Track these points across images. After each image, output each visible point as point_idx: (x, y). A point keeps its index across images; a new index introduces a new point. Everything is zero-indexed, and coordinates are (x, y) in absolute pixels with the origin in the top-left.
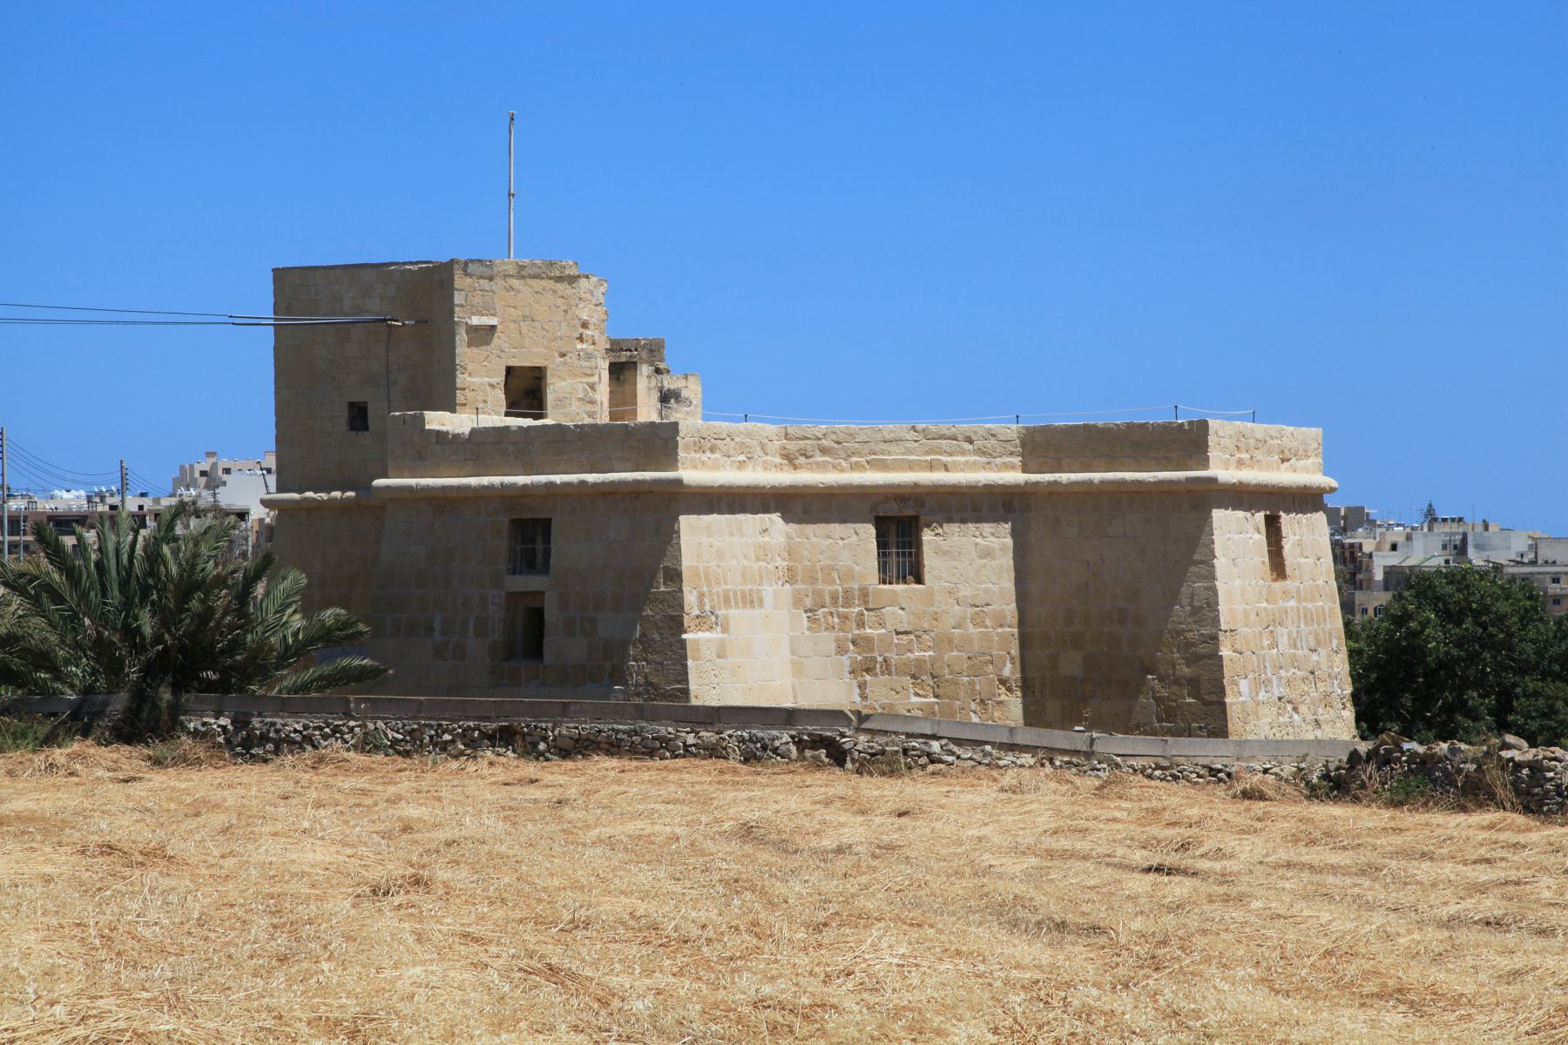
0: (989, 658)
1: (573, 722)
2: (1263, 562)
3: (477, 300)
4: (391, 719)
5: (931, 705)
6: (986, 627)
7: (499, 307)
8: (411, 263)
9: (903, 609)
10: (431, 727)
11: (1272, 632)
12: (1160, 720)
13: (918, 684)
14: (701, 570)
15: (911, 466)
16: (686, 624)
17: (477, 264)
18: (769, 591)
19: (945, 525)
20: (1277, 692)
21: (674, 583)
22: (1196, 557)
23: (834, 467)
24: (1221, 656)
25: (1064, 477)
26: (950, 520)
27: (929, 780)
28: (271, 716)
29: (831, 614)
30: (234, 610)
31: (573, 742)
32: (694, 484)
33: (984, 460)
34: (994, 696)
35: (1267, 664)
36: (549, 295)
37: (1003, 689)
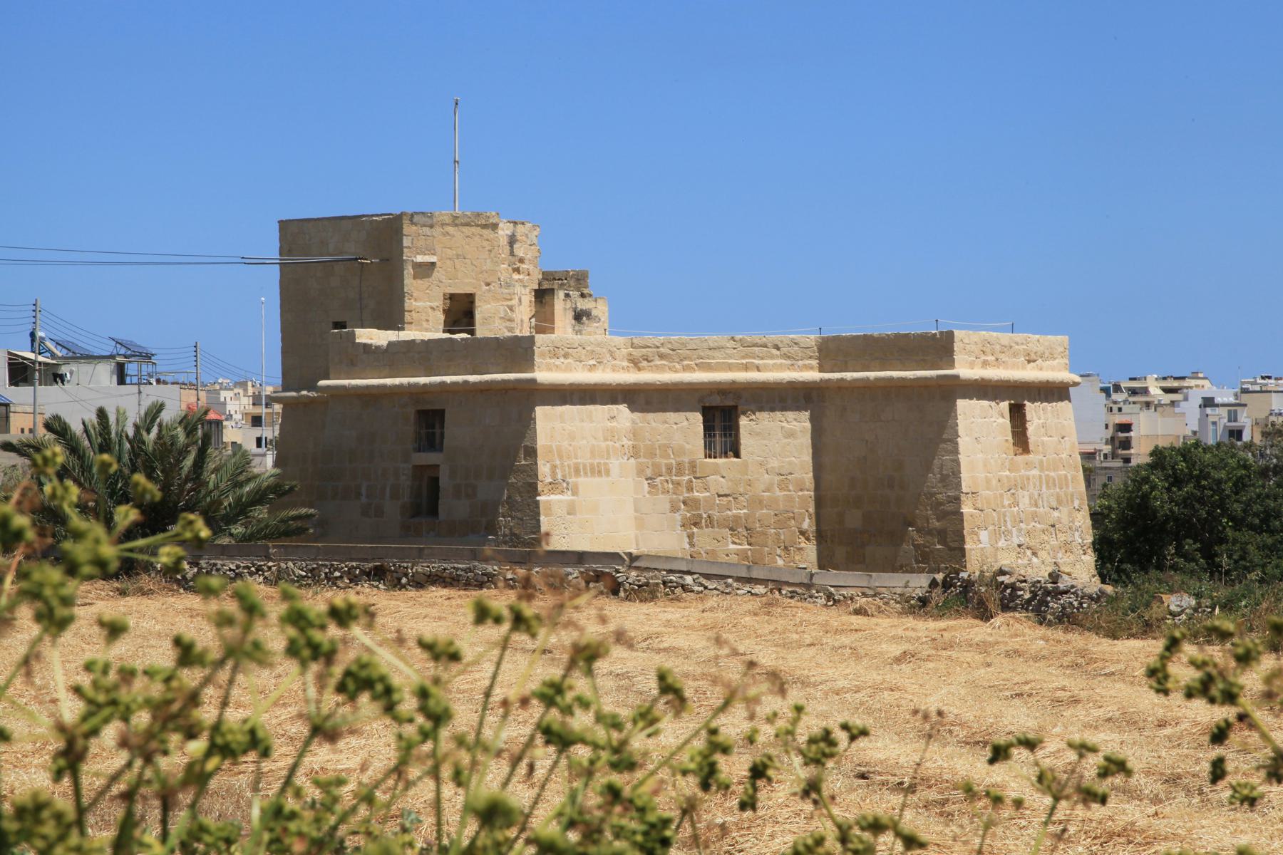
0: (792, 515)
1: (426, 562)
2: (1007, 440)
3: (421, 243)
4: (297, 560)
5: (745, 551)
6: (790, 491)
7: (438, 248)
8: (377, 215)
9: (723, 477)
10: (326, 566)
11: (1013, 494)
12: (918, 562)
13: (735, 535)
14: (554, 447)
15: (730, 368)
16: (540, 489)
17: (421, 215)
18: (615, 464)
19: (757, 413)
20: (1016, 541)
21: (531, 458)
22: (945, 436)
23: (670, 369)
24: (962, 513)
25: (849, 375)
26: (761, 409)
27: (668, 603)
28: (214, 559)
29: (667, 481)
30: (192, 479)
31: (426, 577)
32: (546, 382)
33: (789, 362)
34: (795, 544)
35: (1007, 519)
36: (477, 239)
37: (803, 539)
